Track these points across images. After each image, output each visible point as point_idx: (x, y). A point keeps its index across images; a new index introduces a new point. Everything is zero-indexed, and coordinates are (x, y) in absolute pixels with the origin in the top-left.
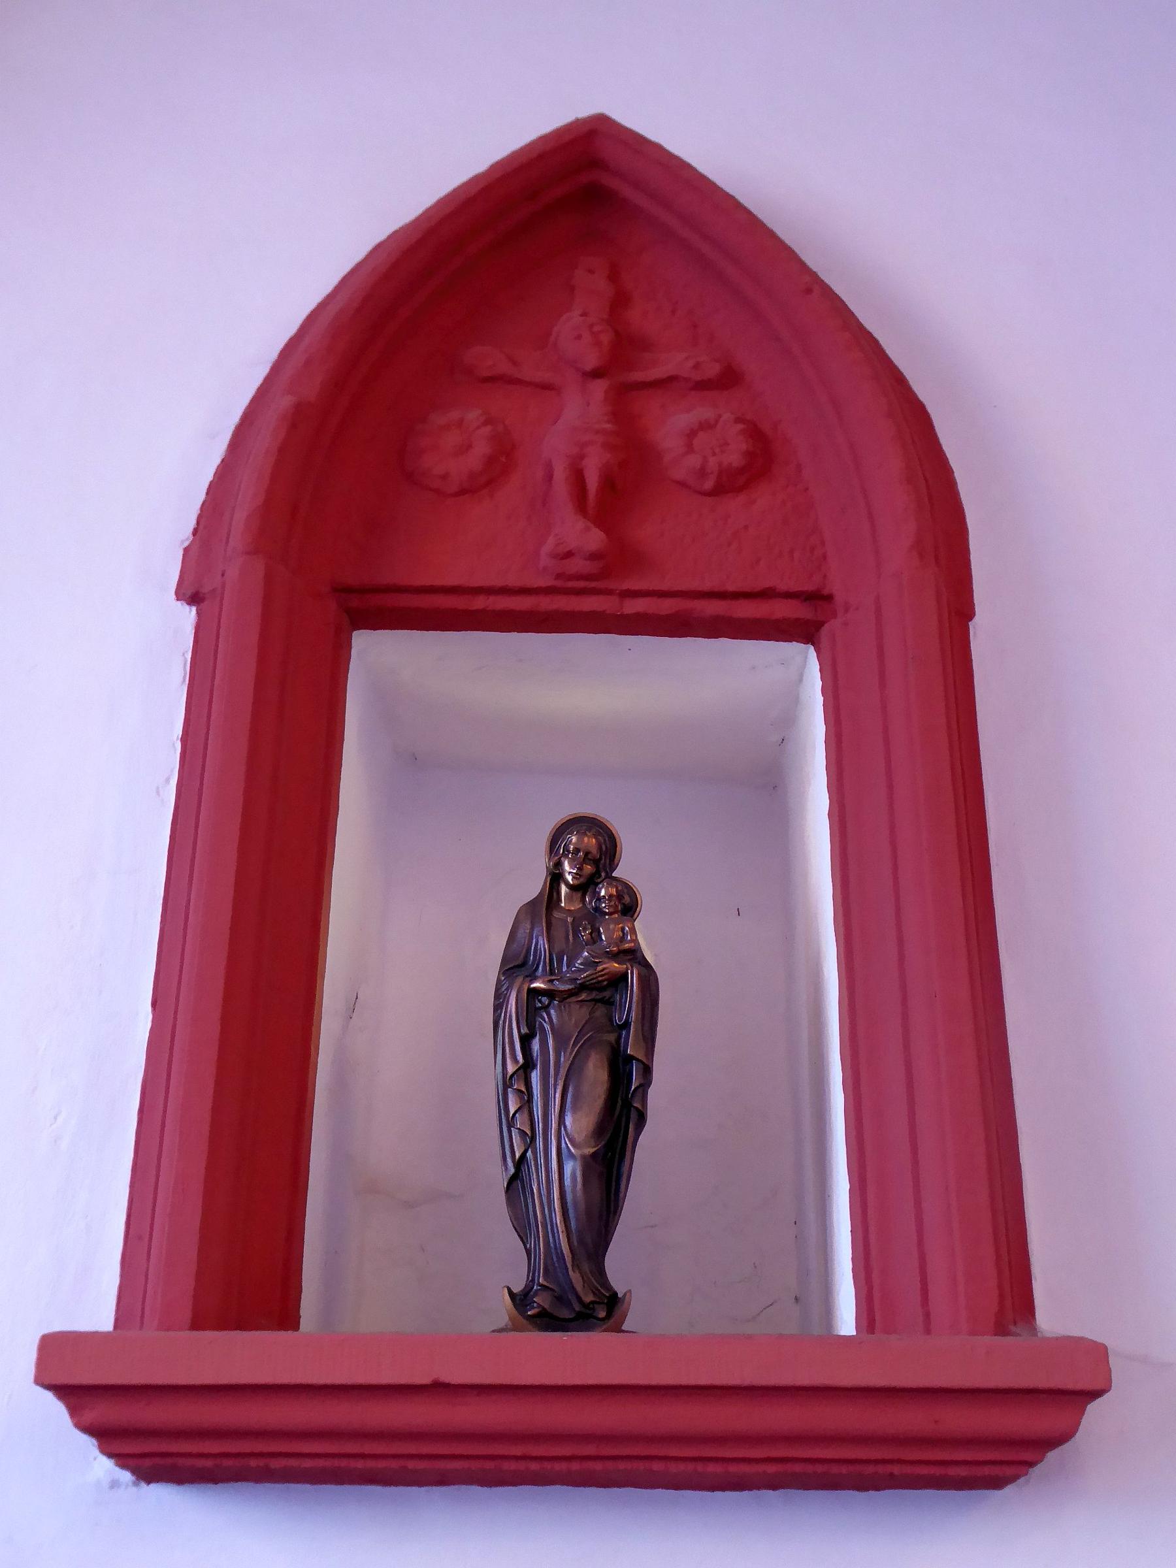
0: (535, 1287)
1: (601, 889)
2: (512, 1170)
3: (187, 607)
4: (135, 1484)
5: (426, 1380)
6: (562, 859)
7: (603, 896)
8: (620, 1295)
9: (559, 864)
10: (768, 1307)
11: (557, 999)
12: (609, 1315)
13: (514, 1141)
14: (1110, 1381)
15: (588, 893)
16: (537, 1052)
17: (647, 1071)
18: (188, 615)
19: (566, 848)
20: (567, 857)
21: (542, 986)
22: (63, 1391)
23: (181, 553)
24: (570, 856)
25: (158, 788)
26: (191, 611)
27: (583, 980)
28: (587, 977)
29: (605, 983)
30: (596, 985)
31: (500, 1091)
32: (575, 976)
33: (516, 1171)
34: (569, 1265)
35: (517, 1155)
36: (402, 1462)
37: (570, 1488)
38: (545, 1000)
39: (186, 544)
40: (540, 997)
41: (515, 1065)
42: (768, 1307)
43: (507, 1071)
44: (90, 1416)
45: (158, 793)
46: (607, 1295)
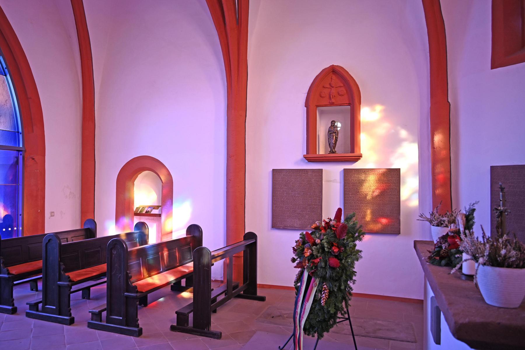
17: (338, 138)
18: (306, 108)
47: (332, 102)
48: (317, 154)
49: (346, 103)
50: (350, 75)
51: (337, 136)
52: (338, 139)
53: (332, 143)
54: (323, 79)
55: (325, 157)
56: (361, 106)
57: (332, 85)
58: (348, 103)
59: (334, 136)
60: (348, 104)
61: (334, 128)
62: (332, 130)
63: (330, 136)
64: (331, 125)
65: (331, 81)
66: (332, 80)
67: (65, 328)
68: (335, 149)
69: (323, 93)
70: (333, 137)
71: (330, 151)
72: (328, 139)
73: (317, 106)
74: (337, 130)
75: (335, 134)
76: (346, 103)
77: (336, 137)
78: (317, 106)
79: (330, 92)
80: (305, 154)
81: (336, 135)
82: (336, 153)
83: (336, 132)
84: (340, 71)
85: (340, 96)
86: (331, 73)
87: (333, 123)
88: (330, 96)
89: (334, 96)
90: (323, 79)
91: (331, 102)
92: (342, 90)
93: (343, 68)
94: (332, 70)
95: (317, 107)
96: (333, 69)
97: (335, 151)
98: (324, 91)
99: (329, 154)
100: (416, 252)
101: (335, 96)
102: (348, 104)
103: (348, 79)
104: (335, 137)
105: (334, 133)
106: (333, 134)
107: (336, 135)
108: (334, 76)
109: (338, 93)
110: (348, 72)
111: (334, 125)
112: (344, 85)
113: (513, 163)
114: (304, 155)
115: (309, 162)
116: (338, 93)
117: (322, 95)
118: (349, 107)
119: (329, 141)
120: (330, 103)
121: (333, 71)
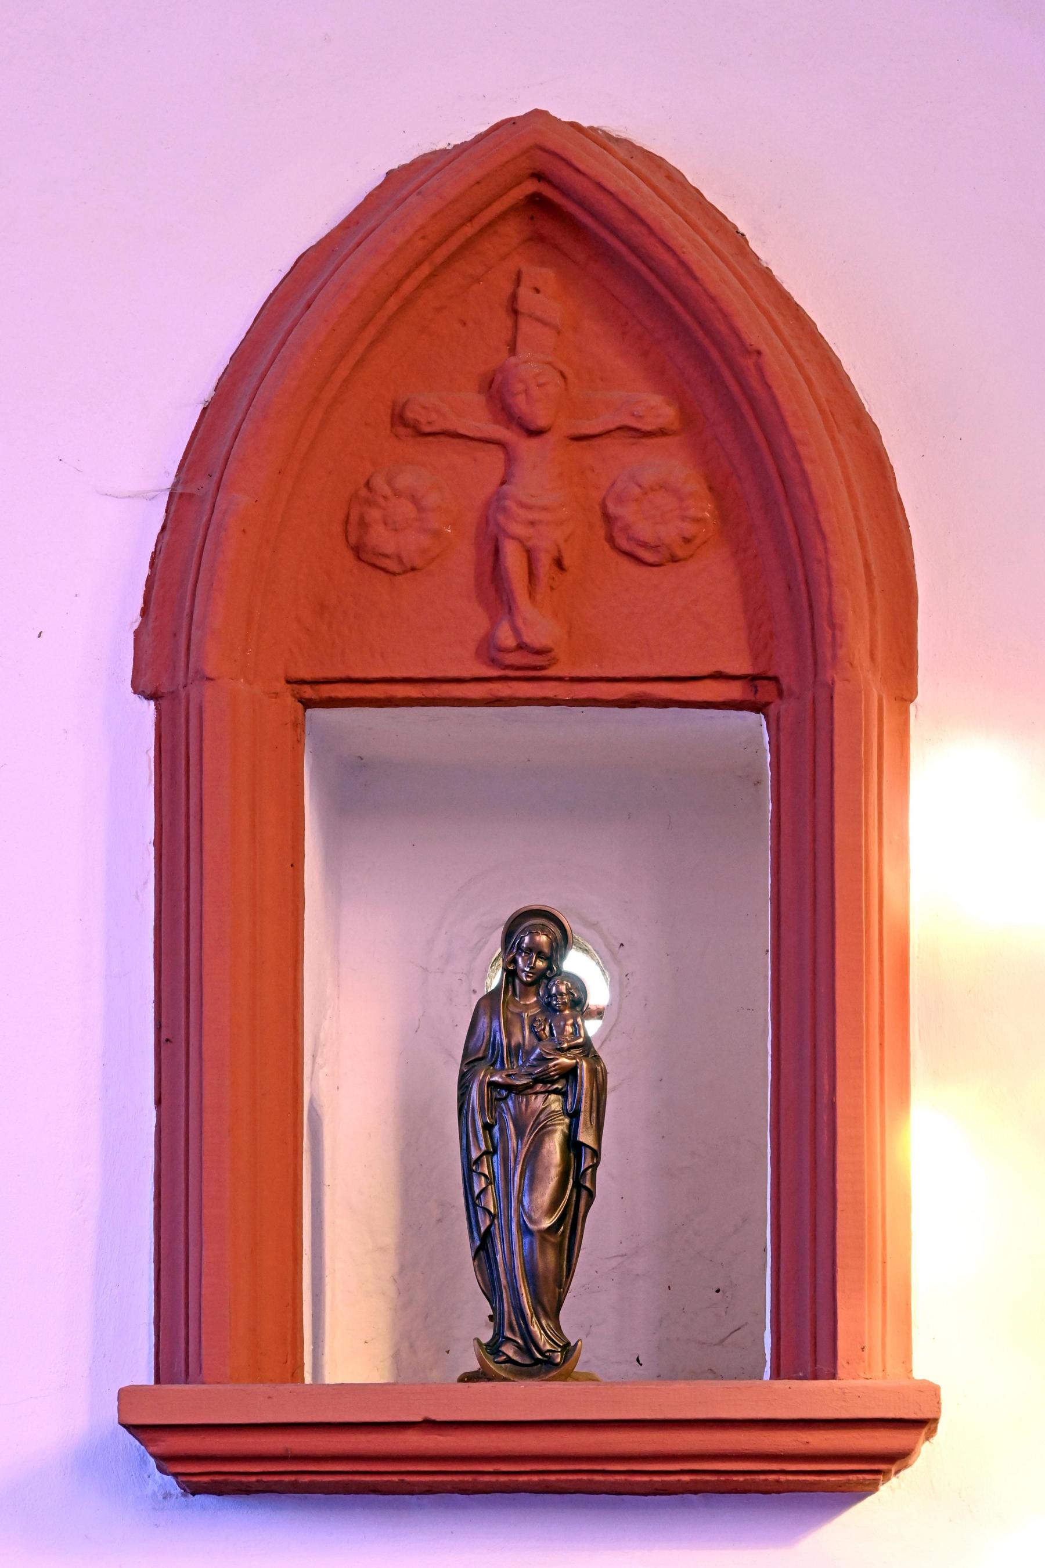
0: (500, 1339)
1: (552, 987)
2: (478, 1243)
3: (146, 702)
4: (184, 1495)
5: (419, 1419)
6: (517, 956)
7: (554, 994)
8: (572, 1344)
9: (514, 961)
10: (736, 1331)
11: (514, 1092)
12: (565, 1359)
13: (479, 1218)
14: (939, 1410)
15: (542, 987)
16: (497, 1140)
17: (596, 1154)
18: (149, 709)
19: (519, 948)
20: (520, 955)
21: (500, 1080)
22: (133, 1429)
23: (132, 637)
24: (523, 955)
25: (137, 892)
26: (149, 704)
27: (537, 1075)
28: (540, 1072)
29: (557, 1077)
30: (512, 1379)
31: (481, 1285)
32: (530, 1070)
33: (481, 1243)
34: (528, 1312)
35: (483, 1230)
36: (401, 1477)
37: (310, 1240)
38: (505, 1093)
39: (136, 626)
40: (498, 1090)
41: (478, 1152)
42: (736, 1331)
43: (471, 1156)
44: (151, 1449)
45: (137, 897)
46: (561, 1345)
47: (521, 647)
48: (308, 1379)
49: (718, 676)
50: (766, 275)
51: (585, 1137)
52: (605, 1179)
53: (525, 1231)
54: (393, 304)
55: (429, 1425)
56: (919, 714)
57: (520, 404)
58: (742, 666)
59: (543, 1132)
60: (734, 691)
61: (549, 1008)
62: (522, 1036)
63: (488, 1127)
64: (511, 974)
65: (513, 350)
66: (526, 326)
67: (597, 1047)
68: (555, 1316)
69: (405, 509)
70: (528, 1139)
71: (493, 1348)
72: (470, 1170)
73: (308, 692)
74: (586, 1048)
75: (555, 1103)
76: (718, 676)
77: (572, 1145)
78: (308, 692)
79: (495, 503)
80: (143, 1375)
81: (574, 1116)
82: (568, 1376)
83: (570, 1074)
84: (632, 213)
85: (628, 567)
86: (513, 231)
87: (534, 950)
88: (497, 551)
89: (545, 564)
90: (393, 304)
91: (505, 637)
92: (663, 486)
93: (674, 177)
94: (531, 187)
95: (308, 704)
96: (538, 176)
97: (568, 1349)
98: (405, 480)
99: (469, 1378)
100: (784, 1492)
101: (559, 563)
102: (734, 691)
103: (754, 338)
104: (554, 1147)
105: (543, 1080)
106: (537, 1102)
107: (574, 1116)
108: (546, 276)
109: (608, 519)
110: (739, 241)
111: (544, 978)
112: (689, 418)
113: (193, 1045)
114: (126, 1395)
115: (193, 1489)
116: (608, 519)
117: (381, 538)
118: (756, 721)
119: (472, 1201)
120: (493, 662)
121: (537, 203)
